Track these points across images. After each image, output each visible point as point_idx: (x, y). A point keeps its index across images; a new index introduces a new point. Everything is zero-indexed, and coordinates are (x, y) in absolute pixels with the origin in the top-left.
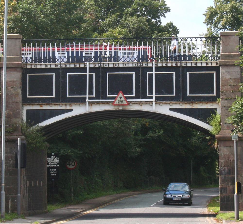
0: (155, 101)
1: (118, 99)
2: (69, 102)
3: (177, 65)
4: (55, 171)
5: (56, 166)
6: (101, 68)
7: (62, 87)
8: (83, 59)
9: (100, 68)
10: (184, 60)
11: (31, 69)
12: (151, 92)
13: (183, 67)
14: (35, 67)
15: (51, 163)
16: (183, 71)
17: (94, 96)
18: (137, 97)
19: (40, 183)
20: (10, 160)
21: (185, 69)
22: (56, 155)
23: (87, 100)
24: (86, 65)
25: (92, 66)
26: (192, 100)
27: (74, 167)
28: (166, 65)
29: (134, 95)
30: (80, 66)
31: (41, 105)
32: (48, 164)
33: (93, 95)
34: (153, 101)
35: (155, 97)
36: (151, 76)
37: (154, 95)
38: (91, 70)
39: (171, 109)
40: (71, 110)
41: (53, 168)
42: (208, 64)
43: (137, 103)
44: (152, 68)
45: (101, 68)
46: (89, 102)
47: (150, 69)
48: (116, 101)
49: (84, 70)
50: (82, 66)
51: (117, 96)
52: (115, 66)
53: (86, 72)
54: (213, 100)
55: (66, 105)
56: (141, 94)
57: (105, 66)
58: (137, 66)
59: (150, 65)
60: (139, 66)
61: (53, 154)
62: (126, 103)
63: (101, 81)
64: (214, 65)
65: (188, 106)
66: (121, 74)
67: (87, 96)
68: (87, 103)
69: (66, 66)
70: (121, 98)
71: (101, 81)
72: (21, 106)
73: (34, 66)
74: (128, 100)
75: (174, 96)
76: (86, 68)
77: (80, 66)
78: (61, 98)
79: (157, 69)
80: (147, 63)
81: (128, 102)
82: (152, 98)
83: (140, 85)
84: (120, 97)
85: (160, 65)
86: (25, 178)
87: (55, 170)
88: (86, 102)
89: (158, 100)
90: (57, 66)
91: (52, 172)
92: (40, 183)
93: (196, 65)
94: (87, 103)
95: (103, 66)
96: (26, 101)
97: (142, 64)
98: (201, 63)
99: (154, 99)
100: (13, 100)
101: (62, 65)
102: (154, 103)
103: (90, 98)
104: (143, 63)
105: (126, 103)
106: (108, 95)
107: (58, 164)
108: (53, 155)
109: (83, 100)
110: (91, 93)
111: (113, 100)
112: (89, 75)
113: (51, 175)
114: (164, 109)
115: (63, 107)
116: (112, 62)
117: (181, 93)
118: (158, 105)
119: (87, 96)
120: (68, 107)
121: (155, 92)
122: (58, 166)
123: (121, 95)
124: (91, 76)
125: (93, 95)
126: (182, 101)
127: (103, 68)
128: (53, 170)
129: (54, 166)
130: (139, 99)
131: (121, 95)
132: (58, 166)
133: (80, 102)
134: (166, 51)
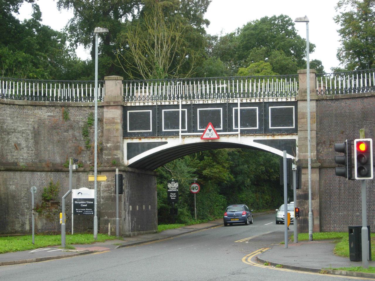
0: (240, 134)
1: (207, 132)
2: (164, 135)
3: (260, 101)
4: (174, 195)
5: (175, 190)
6: (192, 105)
7: (158, 122)
8: (340, 91)
9: (191, 105)
10: (239, 97)
11: (131, 106)
12: (236, 125)
13: (265, 103)
14: (135, 105)
15: (171, 188)
16: (265, 106)
17: (186, 130)
18: (224, 130)
19: (147, 207)
20: (112, 188)
21: (267, 105)
22: (176, 181)
23: (180, 134)
24: (179, 103)
25: (184, 103)
26: (273, 132)
27: (198, 190)
28: (250, 101)
29: (222, 129)
30: (173, 103)
31: (140, 139)
32: (168, 189)
33: (185, 129)
34: (238, 134)
35: (241, 130)
36: (236, 111)
37: (239, 128)
38: (183, 106)
39: (255, 141)
40: (166, 143)
41: (173, 192)
42: (288, 99)
43: (224, 136)
44: (237, 104)
45: (192, 105)
46: (182, 135)
47: (236, 105)
48: (205, 134)
49: (177, 106)
50: (176, 103)
51: (205, 129)
52: (205, 103)
53: (179, 109)
54: (295, 131)
55: (162, 138)
56: (228, 127)
57: (196, 103)
58: (224, 102)
59: (235, 101)
60: (226, 102)
61: (173, 180)
62: (216, 137)
63: (157, 117)
64: (293, 100)
65: (270, 138)
66: (210, 110)
67: (180, 130)
68: (180, 136)
69: (161, 103)
70: (210, 130)
71: (157, 117)
72: (122, 139)
73: (134, 104)
74: (218, 133)
75: (257, 129)
76: (179, 105)
77: (173, 103)
78: (157, 132)
79: (242, 104)
80: (269, 98)
81: (219, 135)
82: (237, 131)
83: (227, 119)
84: (210, 132)
85: (244, 101)
86: (126, 204)
87: (175, 194)
88: (179, 135)
89: (243, 133)
90: (154, 103)
91: (172, 196)
92: (147, 207)
93: (276, 101)
94: (180, 136)
95: (194, 103)
96: (126, 135)
97: (228, 101)
98: (139, 102)
99: (239, 132)
100: (114, 135)
101: (158, 103)
102: (239, 135)
103: (182, 132)
104: (229, 100)
105: (216, 137)
106: (198, 129)
107: (177, 188)
108: (173, 181)
109: (176, 134)
110: (183, 127)
111: (202, 134)
112: (182, 111)
113: (172, 198)
114: (249, 141)
115: (159, 140)
116: (211, 99)
117: (264, 126)
118: (243, 137)
119: (180, 130)
120: (164, 140)
121: (241, 125)
122: (177, 190)
123: (210, 127)
124: (183, 113)
125: (185, 129)
126: (265, 133)
127: (230, 104)
128: (173, 194)
129: (174, 190)
130: (226, 131)
131: (210, 127)
132: (177, 190)
133: (173, 135)
134: (262, 88)
